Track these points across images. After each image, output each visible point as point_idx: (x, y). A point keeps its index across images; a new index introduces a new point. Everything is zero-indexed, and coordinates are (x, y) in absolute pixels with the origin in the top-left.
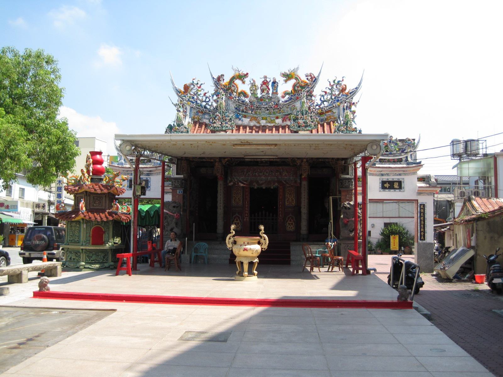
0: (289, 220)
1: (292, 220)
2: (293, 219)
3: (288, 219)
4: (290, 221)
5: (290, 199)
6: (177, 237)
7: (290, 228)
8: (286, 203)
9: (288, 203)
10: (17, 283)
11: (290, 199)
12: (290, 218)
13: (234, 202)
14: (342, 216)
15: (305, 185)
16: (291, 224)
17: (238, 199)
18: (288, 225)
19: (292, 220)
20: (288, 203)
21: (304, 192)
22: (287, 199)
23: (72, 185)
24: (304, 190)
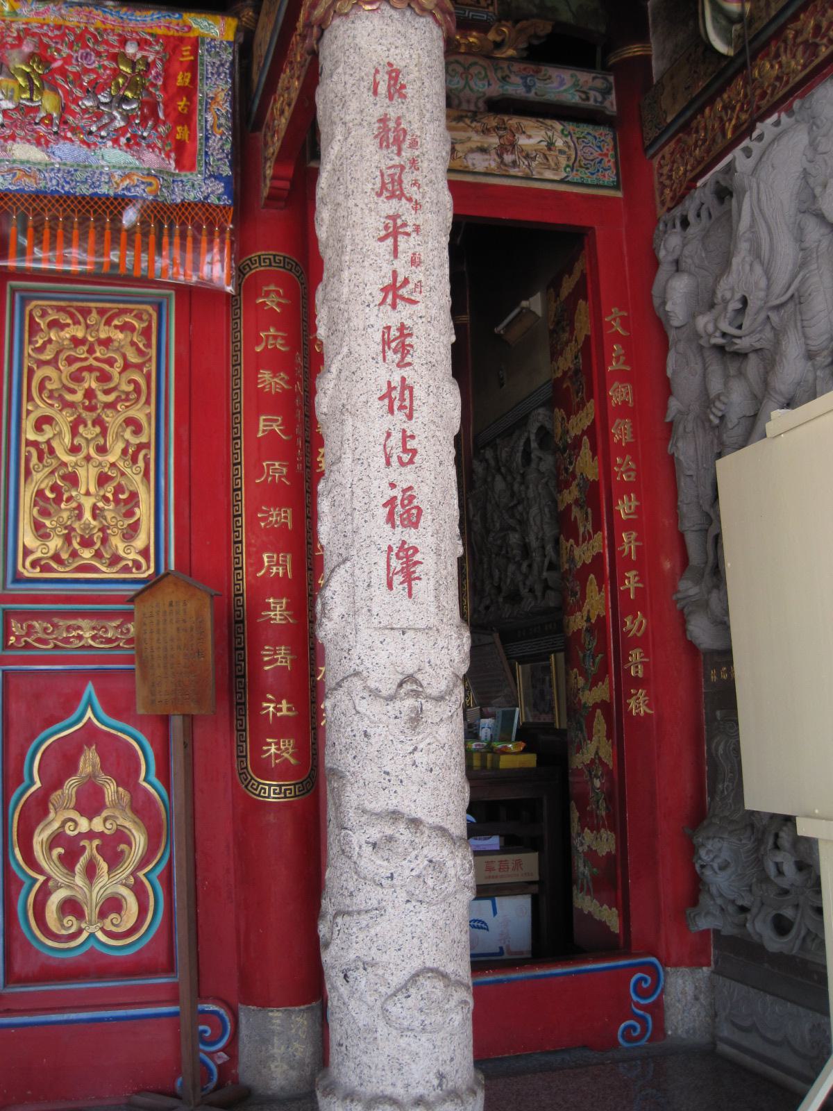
0: (71, 786)
1: (111, 789)
2: (127, 777)
3: (53, 783)
4: (91, 803)
5: (89, 477)
6: (256, 708)
7: (91, 911)
8: (27, 538)
9: (55, 543)
10: (730, 664)
11: (89, 477)
12: (89, 761)
13: (38, 527)
14: (29, 1092)
15: (396, 87)
16: (91, 847)
17: (103, 480)
18: (49, 863)
19: (111, 789)
20: (55, 543)
21: (394, 230)
22: (41, 479)
23: (723, 296)
24: (392, 188)
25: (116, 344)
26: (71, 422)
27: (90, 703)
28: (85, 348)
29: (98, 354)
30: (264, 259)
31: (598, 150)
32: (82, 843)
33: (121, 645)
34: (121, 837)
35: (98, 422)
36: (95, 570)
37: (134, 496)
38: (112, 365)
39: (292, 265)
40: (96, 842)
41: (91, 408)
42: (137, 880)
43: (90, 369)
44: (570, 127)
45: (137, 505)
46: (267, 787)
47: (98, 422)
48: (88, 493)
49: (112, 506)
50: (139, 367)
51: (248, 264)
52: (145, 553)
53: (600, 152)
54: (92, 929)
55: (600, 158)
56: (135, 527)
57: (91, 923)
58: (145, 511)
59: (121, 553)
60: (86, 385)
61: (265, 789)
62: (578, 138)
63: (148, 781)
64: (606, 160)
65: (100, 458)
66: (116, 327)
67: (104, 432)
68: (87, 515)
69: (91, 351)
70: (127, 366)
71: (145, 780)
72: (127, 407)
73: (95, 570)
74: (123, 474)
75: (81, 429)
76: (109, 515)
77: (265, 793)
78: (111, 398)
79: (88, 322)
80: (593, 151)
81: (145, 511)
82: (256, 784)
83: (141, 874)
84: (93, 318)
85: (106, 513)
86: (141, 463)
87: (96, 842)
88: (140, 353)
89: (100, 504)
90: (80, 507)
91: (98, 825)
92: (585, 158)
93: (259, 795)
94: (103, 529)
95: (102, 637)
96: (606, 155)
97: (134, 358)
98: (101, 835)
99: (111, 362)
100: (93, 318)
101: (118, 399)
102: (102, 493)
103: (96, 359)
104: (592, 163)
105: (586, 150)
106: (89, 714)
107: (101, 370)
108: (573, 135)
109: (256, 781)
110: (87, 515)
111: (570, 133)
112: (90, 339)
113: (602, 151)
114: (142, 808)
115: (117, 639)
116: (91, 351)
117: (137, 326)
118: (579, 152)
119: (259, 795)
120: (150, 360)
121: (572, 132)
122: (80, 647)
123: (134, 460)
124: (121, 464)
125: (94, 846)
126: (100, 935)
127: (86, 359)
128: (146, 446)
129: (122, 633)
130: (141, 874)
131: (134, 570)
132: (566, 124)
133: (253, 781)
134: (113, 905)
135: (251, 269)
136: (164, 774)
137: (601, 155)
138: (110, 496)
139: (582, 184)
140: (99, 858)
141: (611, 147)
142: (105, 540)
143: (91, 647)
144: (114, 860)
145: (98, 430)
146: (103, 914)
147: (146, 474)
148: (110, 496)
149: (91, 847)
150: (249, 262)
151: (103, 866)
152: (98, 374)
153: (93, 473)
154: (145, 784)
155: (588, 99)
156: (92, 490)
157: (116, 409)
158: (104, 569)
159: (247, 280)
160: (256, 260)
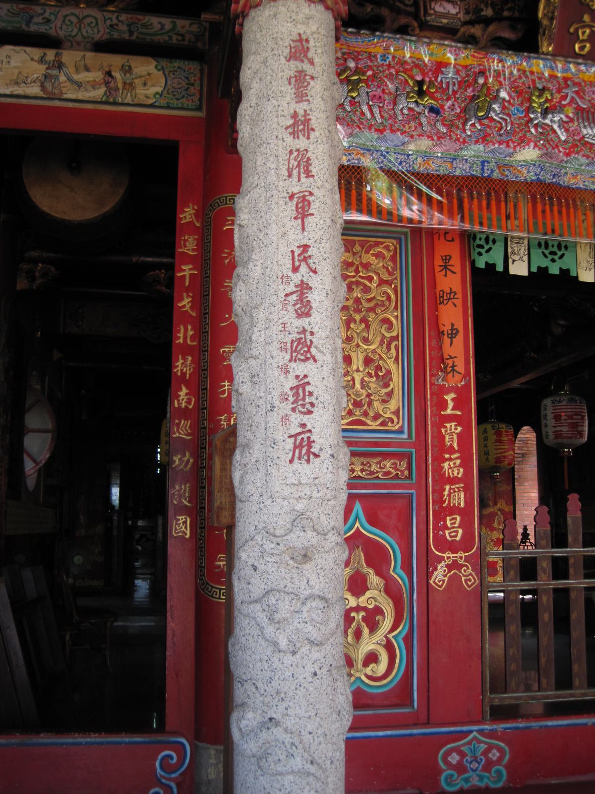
17: (368, 361)
19: (374, 579)
25: (373, 267)
26: (345, 320)
27: (357, 518)
28: (353, 268)
29: (361, 274)
30: (230, 199)
31: (186, 80)
32: (352, 614)
33: (380, 476)
34: (378, 611)
35: (364, 320)
36: (364, 424)
37: (389, 372)
38: (370, 282)
39: (221, 202)
40: (362, 614)
41: (357, 311)
42: (388, 640)
43: (358, 283)
44: (164, 62)
45: (391, 380)
46: (218, 591)
47: (364, 320)
48: (358, 370)
49: (374, 379)
50: (389, 283)
51: (217, 202)
52: (396, 413)
53: (187, 82)
54: (358, 675)
55: (187, 86)
56: (390, 394)
57: (357, 671)
58: (396, 383)
59: (381, 412)
60: (355, 295)
61: (217, 592)
62: (170, 72)
63: (397, 573)
64: (192, 88)
65: (366, 347)
66: (373, 255)
67: (368, 326)
68: (358, 386)
69: (357, 271)
70: (382, 282)
71: (394, 570)
72: (382, 311)
73: (364, 424)
74: (381, 358)
75: (352, 326)
76: (373, 386)
77: (216, 594)
78: (372, 304)
79: (354, 250)
80: (181, 81)
81: (396, 383)
82: (210, 588)
83: (390, 636)
84: (357, 248)
85: (370, 384)
86: (393, 351)
87: (362, 614)
88: (390, 274)
89: (366, 379)
90: (353, 380)
91: (362, 601)
92: (173, 88)
93: (212, 596)
94: (369, 395)
95: (367, 470)
96: (193, 85)
97: (386, 277)
98: (365, 609)
99: (370, 279)
100: (357, 248)
101: (377, 305)
102: (367, 371)
103: (360, 277)
104: (179, 91)
105: (176, 81)
106: (357, 524)
107: (365, 286)
108: (165, 69)
109: (210, 585)
110: (358, 386)
111: (163, 68)
112: (357, 263)
113: (189, 80)
114: (391, 590)
115: (378, 472)
116: (357, 271)
117: (386, 255)
118: (169, 82)
119: (212, 596)
120: (396, 279)
121: (165, 67)
122: (375, 478)
123: (389, 348)
124: (379, 351)
125: (360, 617)
126: (363, 678)
127: (354, 277)
128: (396, 338)
129: (380, 468)
130: (390, 636)
131: (389, 424)
132: (160, 60)
133: (208, 586)
134: (372, 658)
135: (219, 206)
136: (407, 567)
137: (187, 84)
138: (373, 372)
139: (183, 109)
140: (363, 624)
141: (197, 78)
142: (370, 404)
143: (360, 477)
144: (373, 627)
145: (363, 325)
146: (366, 664)
147: (397, 359)
148: (373, 372)
149: (359, 616)
150: (218, 200)
151: (366, 631)
152: (362, 287)
153: (361, 357)
154: (392, 574)
155: (184, 40)
156: (361, 369)
157: (375, 312)
158: (371, 423)
159: (216, 212)
160: (223, 200)
